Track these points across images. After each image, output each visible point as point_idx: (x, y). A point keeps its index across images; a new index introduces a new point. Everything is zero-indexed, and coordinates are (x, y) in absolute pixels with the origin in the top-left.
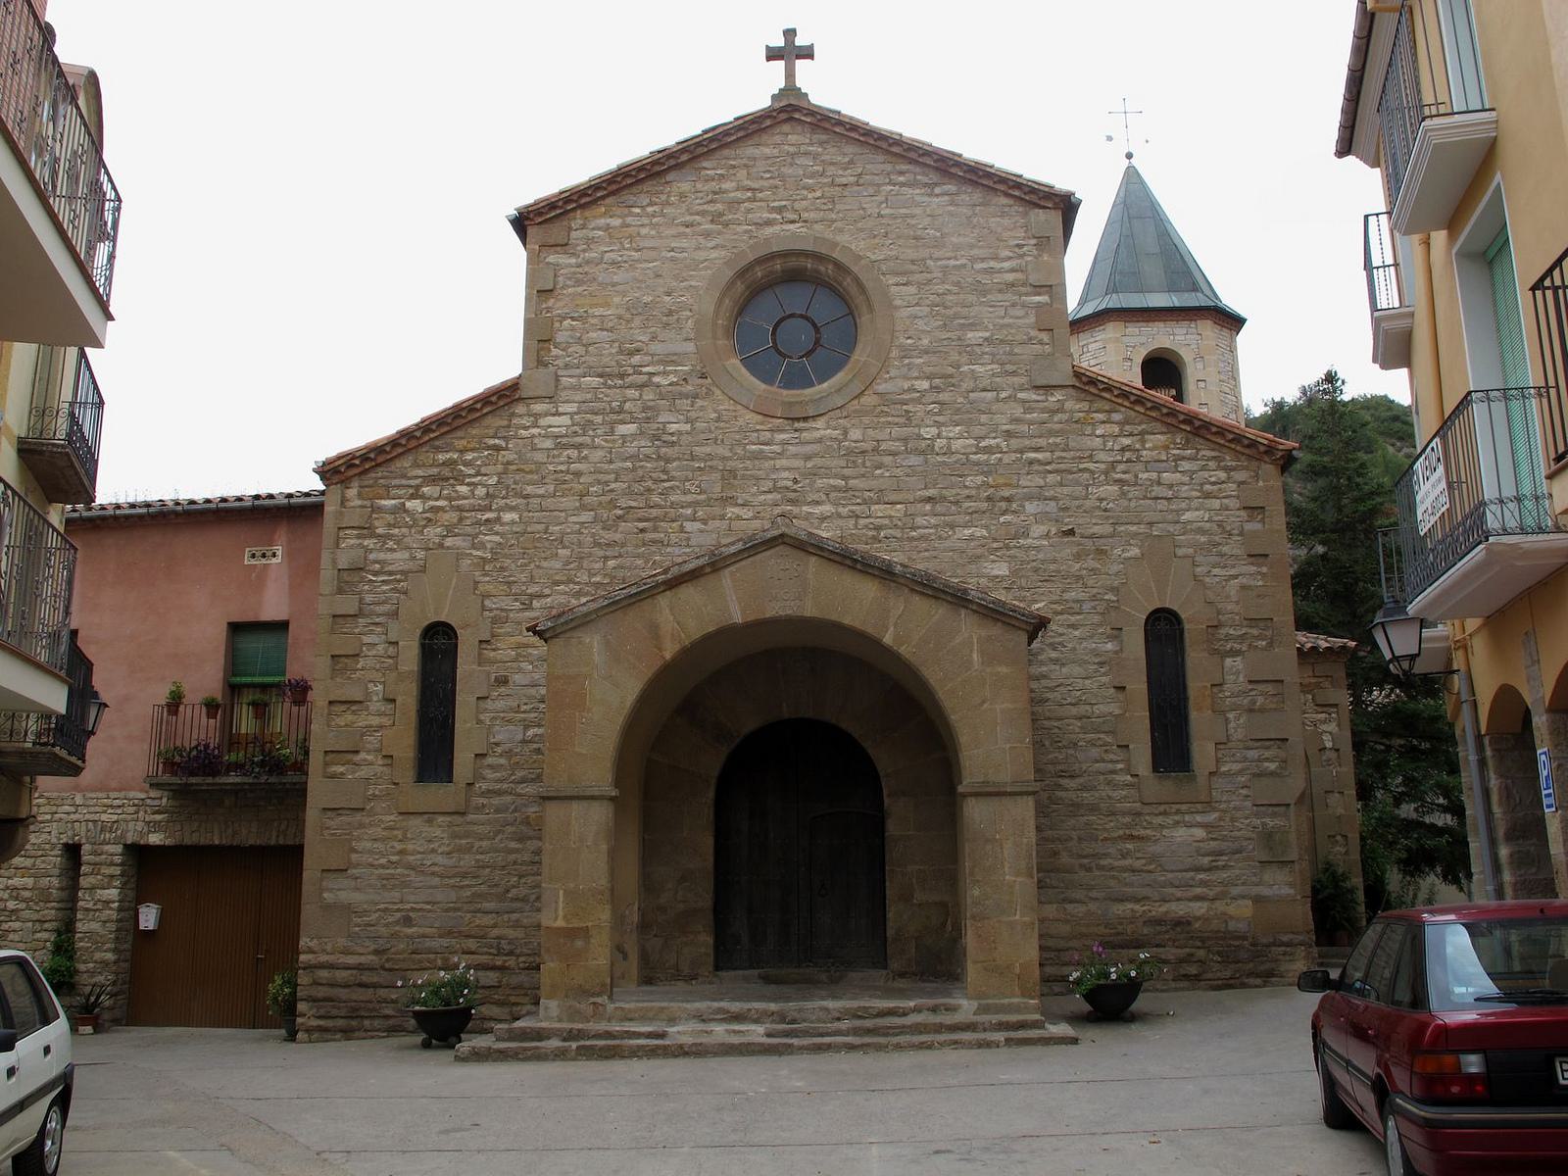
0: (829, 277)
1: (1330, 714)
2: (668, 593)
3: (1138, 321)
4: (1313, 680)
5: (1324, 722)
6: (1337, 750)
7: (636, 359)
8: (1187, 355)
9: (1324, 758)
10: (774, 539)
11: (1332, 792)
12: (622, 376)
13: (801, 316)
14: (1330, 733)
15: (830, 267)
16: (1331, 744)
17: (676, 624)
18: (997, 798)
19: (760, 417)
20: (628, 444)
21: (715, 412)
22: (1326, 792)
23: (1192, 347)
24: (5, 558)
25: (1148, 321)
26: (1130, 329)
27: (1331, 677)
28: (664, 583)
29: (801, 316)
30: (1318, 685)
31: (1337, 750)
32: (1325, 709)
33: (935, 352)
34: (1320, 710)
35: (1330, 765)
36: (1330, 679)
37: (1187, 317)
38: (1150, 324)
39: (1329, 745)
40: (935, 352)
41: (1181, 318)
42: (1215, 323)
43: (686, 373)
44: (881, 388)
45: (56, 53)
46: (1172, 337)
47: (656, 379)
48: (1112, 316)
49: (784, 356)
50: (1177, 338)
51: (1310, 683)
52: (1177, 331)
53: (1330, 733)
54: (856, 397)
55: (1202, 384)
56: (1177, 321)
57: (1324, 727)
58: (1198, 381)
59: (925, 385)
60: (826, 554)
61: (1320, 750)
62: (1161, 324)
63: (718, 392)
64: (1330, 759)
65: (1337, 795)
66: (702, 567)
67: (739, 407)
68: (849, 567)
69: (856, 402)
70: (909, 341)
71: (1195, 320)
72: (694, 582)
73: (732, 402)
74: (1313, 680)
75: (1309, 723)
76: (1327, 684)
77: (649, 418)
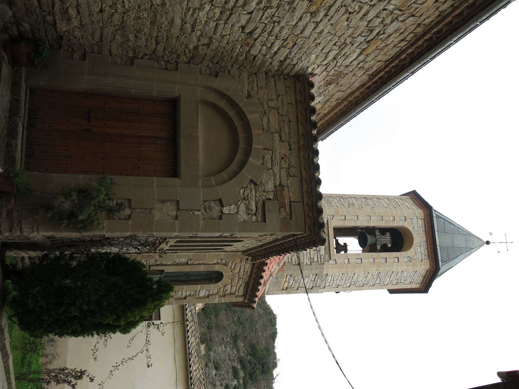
1: (255, 215)
3: (425, 226)
4: (287, 201)
5: (248, 208)
6: (220, 218)
8: (410, 252)
9: (212, 204)
11: (178, 209)
14: (237, 213)
16: (227, 212)
18: (178, 318)
22: (178, 202)
23: (415, 256)
24: (218, 235)
25: (425, 232)
26: (421, 222)
27: (291, 218)
30: (282, 206)
31: (220, 218)
32: (260, 210)
34: (260, 204)
35: (205, 210)
36: (288, 217)
37: (430, 254)
38: (424, 233)
39: (226, 210)
41: (429, 250)
42: (427, 271)
45: (322, 160)
46: (419, 245)
48: (427, 211)
50: (419, 247)
51: (284, 198)
52: (422, 248)
53: (237, 213)
55: (396, 260)
56: (427, 248)
57: (243, 207)
58: (398, 258)
61: (220, 200)
62: (425, 239)
64: (211, 210)
65: (174, 213)
71: (429, 258)
74: (287, 201)
75: (246, 193)
76: (283, 214)
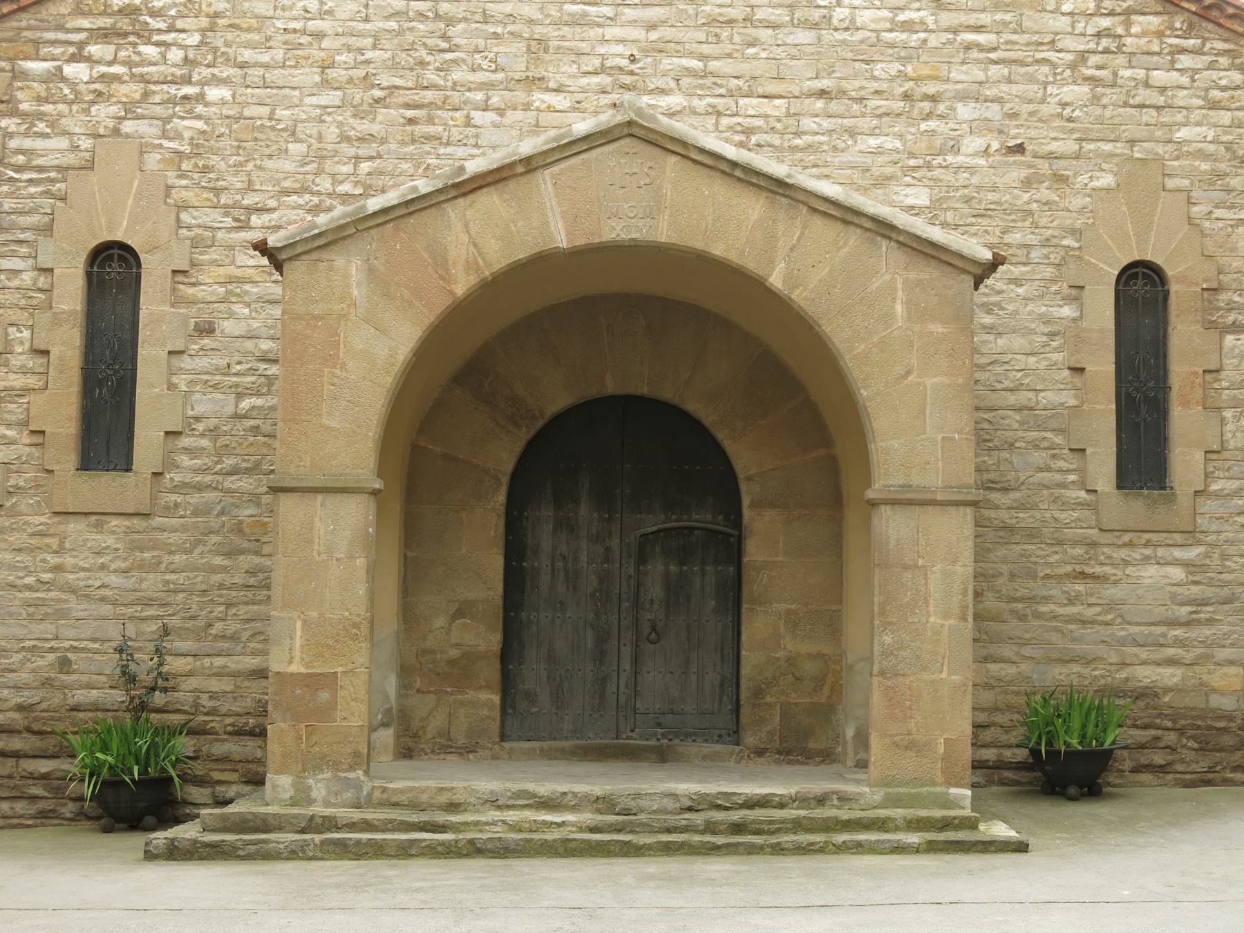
72: (500, 186)
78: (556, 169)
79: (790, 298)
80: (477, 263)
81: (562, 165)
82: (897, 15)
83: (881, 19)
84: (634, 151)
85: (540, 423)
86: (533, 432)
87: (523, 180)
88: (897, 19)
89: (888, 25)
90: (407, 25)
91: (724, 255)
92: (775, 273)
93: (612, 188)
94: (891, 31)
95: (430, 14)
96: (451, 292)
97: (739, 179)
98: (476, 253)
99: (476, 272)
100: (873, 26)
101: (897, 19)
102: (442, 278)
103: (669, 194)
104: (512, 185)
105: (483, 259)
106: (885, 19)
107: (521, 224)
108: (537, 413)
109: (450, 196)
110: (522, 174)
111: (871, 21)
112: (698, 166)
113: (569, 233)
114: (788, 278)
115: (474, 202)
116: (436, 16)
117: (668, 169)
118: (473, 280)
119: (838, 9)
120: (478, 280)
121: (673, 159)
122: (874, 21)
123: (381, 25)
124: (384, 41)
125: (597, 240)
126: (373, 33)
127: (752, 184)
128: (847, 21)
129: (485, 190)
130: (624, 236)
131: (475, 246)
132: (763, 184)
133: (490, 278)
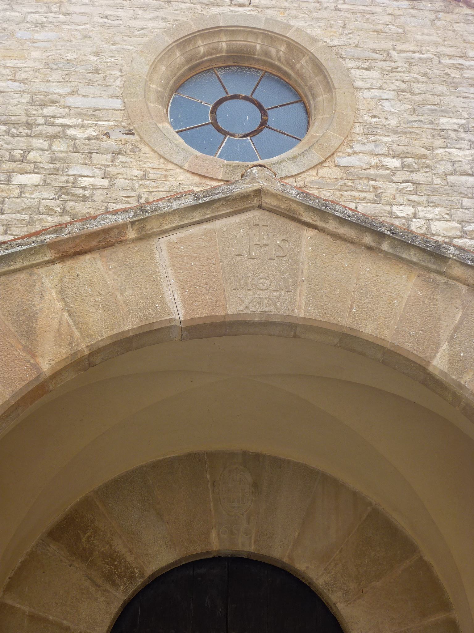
0: (280, 60)
2: (58, 267)
7: (49, 111)
10: (245, 197)
12: (29, 126)
13: (246, 98)
15: (283, 48)
17: (66, 315)
19: (197, 179)
20: (27, 195)
21: (141, 169)
28: (52, 246)
29: (246, 98)
33: (405, 133)
40: (405, 133)
43: (109, 127)
44: (344, 161)
47: (71, 132)
49: (225, 133)
54: (313, 168)
59: (395, 163)
60: (331, 225)
63: (145, 150)
66: (122, 228)
67: (170, 166)
68: (369, 248)
69: (313, 172)
70: (375, 120)
72: (106, 252)
73: (162, 160)
77: (57, 170)
78: (174, 237)
79: (460, 386)
80: (72, 335)
81: (182, 234)
82: (464, 226)
83: (452, 228)
84: (265, 223)
85: (139, 582)
86: (131, 591)
87: (135, 247)
88: (465, 229)
89: (458, 233)
90: (36, 217)
91: (376, 333)
92: (438, 355)
93: (239, 258)
94: (461, 237)
95: (58, 209)
96: (36, 366)
97: (387, 255)
98: (71, 323)
99: (70, 344)
100: (446, 233)
101: (465, 229)
102: (26, 349)
103: (306, 267)
104: (120, 252)
105: (79, 329)
106: (456, 228)
107: (129, 292)
108: (137, 572)
109: (46, 259)
110: (134, 241)
111: (444, 230)
112: (338, 241)
113: (188, 303)
114: (454, 360)
115: (72, 269)
116: (63, 212)
117: (304, 244)
118: (64, 352)
119: (414, 220)
120: (70, 353)
121: (309, 233)
122: (446, 230)
123: (13, 216)
124: (15, 229)
125: (222, 312)
126: (5, 222)
127: (402, 260)
128: (424, 229)
129: (88, 256)
130: (254, 309)
131: (71, 314)
132: (415, 259)
133: (87, 352)
